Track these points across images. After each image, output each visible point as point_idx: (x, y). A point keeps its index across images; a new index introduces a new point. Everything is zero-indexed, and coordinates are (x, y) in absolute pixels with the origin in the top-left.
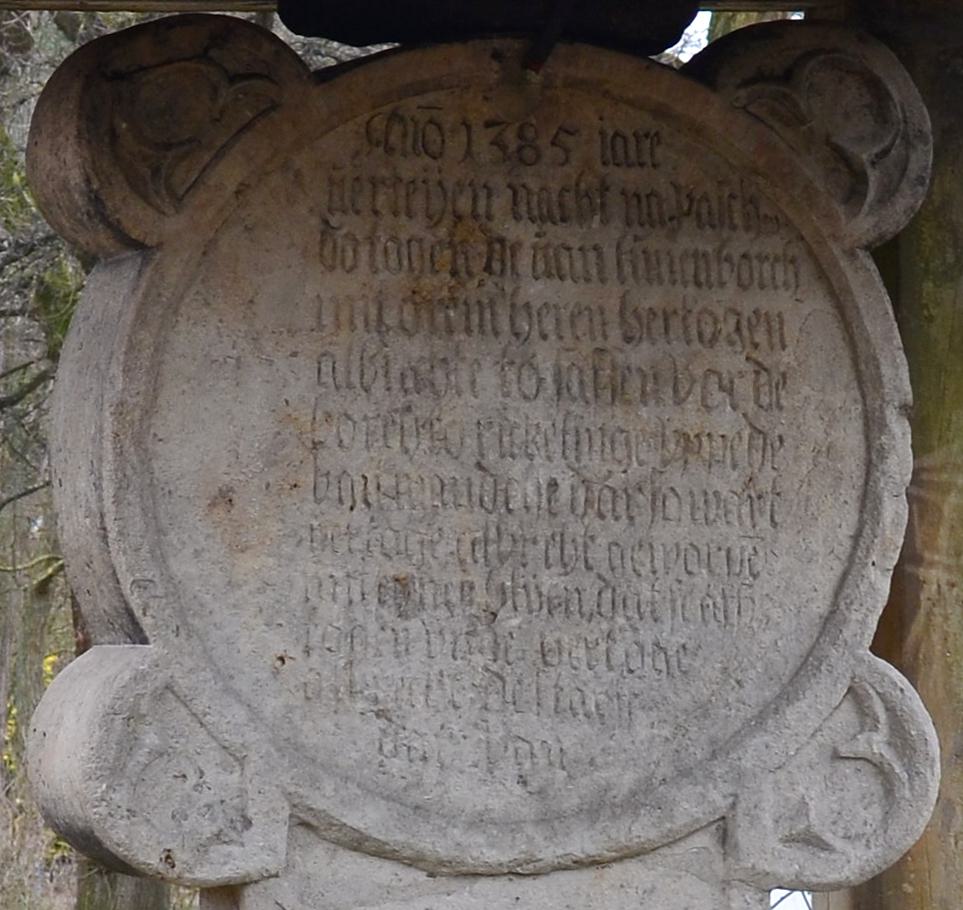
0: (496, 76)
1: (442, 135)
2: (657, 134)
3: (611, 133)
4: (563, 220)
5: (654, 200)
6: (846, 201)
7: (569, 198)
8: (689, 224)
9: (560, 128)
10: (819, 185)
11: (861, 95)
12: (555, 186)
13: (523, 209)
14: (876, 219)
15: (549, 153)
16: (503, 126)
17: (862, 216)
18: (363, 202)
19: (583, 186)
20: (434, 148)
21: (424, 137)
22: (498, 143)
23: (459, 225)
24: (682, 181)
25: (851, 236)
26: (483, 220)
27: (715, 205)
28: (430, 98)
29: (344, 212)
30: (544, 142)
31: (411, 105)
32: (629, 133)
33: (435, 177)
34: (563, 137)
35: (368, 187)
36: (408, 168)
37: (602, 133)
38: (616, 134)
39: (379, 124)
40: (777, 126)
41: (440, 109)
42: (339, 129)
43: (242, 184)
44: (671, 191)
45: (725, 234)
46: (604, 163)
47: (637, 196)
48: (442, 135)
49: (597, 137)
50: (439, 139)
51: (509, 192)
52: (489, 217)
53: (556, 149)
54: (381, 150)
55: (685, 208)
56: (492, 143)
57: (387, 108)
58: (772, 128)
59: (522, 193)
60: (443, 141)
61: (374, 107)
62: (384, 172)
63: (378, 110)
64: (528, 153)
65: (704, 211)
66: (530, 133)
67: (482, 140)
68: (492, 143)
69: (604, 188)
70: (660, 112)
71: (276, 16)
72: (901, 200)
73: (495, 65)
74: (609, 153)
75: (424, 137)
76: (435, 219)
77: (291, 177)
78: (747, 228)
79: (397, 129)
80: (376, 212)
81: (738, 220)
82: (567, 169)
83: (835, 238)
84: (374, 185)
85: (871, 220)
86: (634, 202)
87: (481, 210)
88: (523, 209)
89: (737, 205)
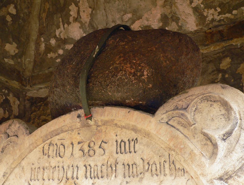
0: (79, 124)
1: (65, 149)
2: (136, 139)
3: (119, 141)
4: (102, 177)
5: (134, 166)
6: (210, 158)
7: (104, 168)
8: (148, 175)
9: (102, 141)
10: (196, 152)
11: (220, 111)
12: (99, 164)
13: (88, 174)
14: (223, 164)
15: (99, 151)
16: (83, 143)
17: (215, 164)
18: (40, 177)
19: (109, 163)
20: (62, 154)
21: (59, 150)
22: (82, 150)
23: (68, 182)
24: (145, 158)
25: (211, 173)
26: (75, 179)
27: (158, 166)
28: (62, 135)
29: (35, 180)
30: (96, 147)
31: (56, 140)
32: (126, 140)
33: (61, 165)
34: (103, 144)
35: (42, 170)
36: (54, 162)
37: (116, 141)
38: (122, 141)
39: (46, 147)
40: (181, 128)
41: (64, 139)
42: (34, 150)
43: (5, 173)
44: (141, 161)
45: (162, 177)
46: (117, 153)
47: (128, 165)
48: (65, 149)
49: (115, 143)
50: (64, 150)
51: (84, 168)
52: (77, 178)
53: (101, 149)
54: (46, 157)
55: (147, 168)
56: (80, 150)
57: (48, 141)
58: (178, 130)
59: (89, 168)
60: (65, 151)
61: (44, 142)
62: (47, 165)
63: (45, 143)
64: (92, 152)
65: (154, 169)
66: (92, 145)
67: (77, 147)
68: (80, 150)
69: (116, 163)
70: (135, 130)
71: (142, 103)
72: (235, 154)
73: (78, 120)
74: (119, 149)
75: (59, 150)
76: (60, 180)
77: (21, 168)
78: (171, 175)
79: (51, 148)
80: (44, 180)
81: (167, 171)
82: (104, 157)
83: (203, 175)
84: (44, 169)
85: (220, 166)
86: (127, 167)
87: (75, 176)
88: (88, 174)
89: (167, 165)
